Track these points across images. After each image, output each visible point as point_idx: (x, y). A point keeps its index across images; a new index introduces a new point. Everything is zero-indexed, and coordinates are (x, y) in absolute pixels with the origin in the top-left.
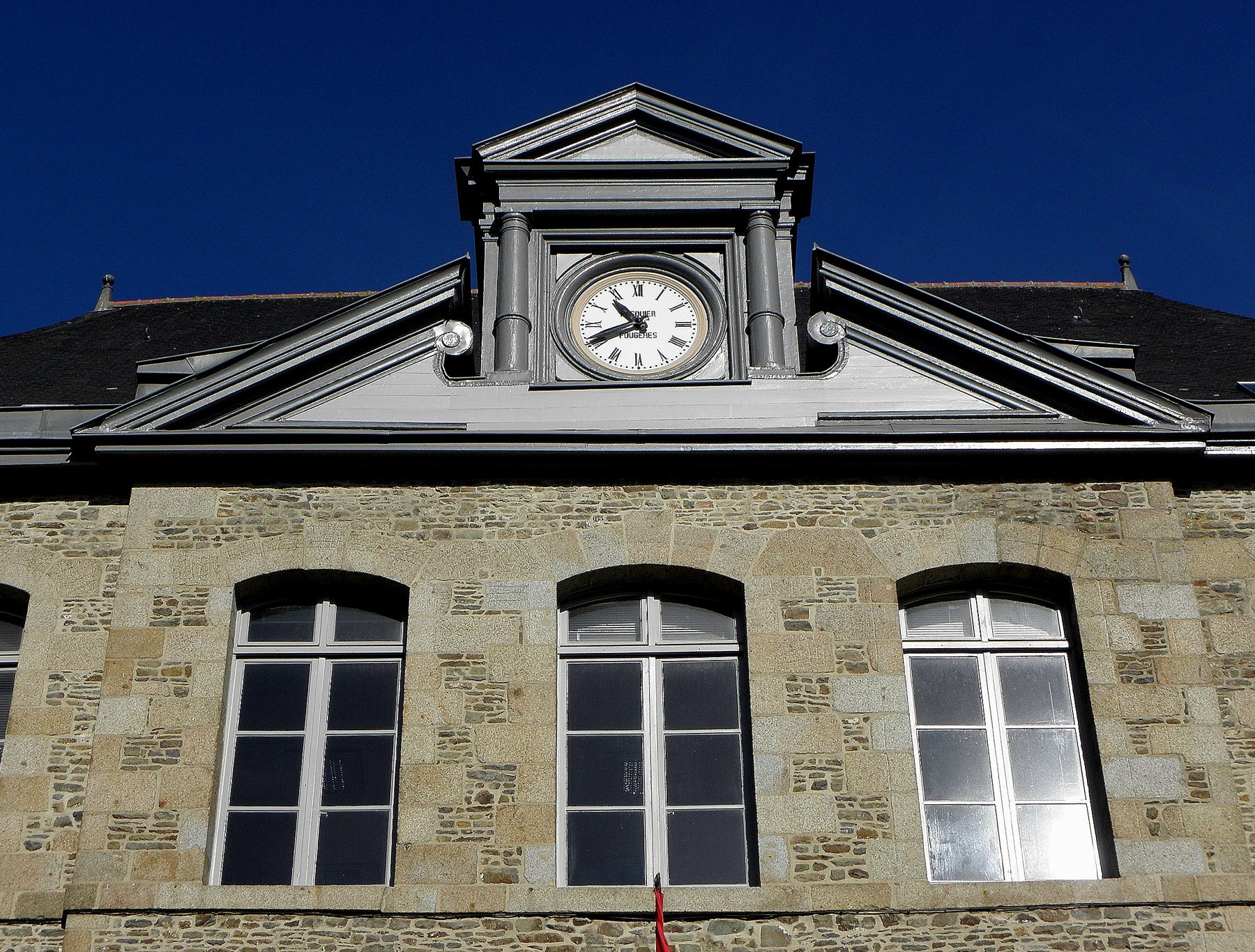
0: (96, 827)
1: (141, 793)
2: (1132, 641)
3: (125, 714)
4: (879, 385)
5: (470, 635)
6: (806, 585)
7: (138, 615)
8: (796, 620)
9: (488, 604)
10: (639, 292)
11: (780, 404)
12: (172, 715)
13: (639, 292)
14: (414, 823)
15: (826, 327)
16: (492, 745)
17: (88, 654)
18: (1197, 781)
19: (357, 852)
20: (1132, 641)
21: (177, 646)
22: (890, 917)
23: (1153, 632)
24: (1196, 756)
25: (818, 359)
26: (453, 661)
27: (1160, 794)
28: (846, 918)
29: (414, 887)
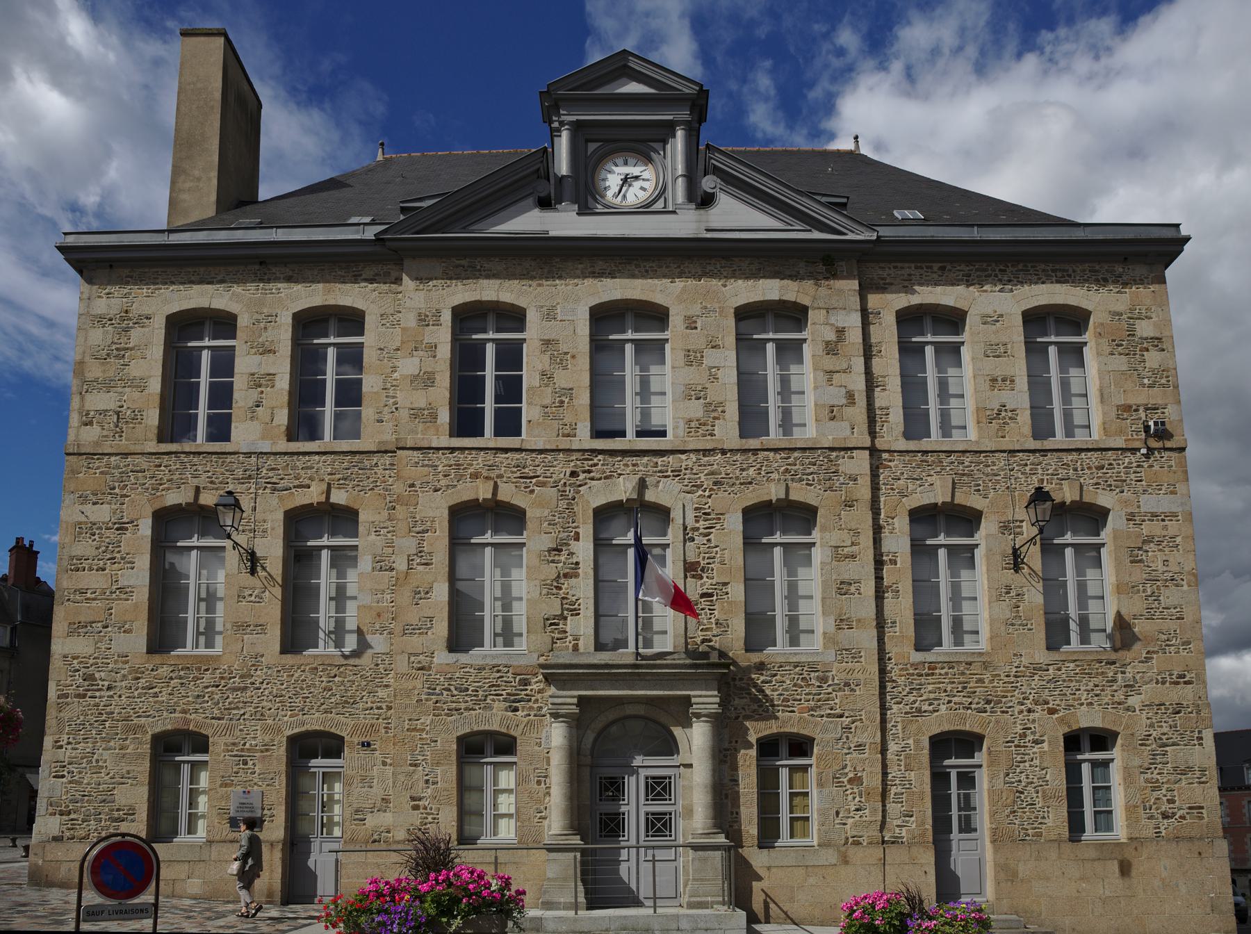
0: (404, 414)
2: (832, 336)
3: (409, 366)
4: (735, 216)
5: (552, 330)
6: (696, 309)
7: (410, 321)
8: (691, 325)
9: (558, 314)
10: (643, 189)
11: (684, 224)
12: (429, 365)
13: (643, 189)
14: (529, 411)
15: (708, 183)
16: (562, 379)
18: (850, 396)
19: (509, 423)
20: (832, 336)
21: (430, 335)
22: (724, 452)
23: (841, 332)
24: (851, 387)
25: (706, 201)
26: (547, 342)
28: (706, 452)
29: (529, 437)
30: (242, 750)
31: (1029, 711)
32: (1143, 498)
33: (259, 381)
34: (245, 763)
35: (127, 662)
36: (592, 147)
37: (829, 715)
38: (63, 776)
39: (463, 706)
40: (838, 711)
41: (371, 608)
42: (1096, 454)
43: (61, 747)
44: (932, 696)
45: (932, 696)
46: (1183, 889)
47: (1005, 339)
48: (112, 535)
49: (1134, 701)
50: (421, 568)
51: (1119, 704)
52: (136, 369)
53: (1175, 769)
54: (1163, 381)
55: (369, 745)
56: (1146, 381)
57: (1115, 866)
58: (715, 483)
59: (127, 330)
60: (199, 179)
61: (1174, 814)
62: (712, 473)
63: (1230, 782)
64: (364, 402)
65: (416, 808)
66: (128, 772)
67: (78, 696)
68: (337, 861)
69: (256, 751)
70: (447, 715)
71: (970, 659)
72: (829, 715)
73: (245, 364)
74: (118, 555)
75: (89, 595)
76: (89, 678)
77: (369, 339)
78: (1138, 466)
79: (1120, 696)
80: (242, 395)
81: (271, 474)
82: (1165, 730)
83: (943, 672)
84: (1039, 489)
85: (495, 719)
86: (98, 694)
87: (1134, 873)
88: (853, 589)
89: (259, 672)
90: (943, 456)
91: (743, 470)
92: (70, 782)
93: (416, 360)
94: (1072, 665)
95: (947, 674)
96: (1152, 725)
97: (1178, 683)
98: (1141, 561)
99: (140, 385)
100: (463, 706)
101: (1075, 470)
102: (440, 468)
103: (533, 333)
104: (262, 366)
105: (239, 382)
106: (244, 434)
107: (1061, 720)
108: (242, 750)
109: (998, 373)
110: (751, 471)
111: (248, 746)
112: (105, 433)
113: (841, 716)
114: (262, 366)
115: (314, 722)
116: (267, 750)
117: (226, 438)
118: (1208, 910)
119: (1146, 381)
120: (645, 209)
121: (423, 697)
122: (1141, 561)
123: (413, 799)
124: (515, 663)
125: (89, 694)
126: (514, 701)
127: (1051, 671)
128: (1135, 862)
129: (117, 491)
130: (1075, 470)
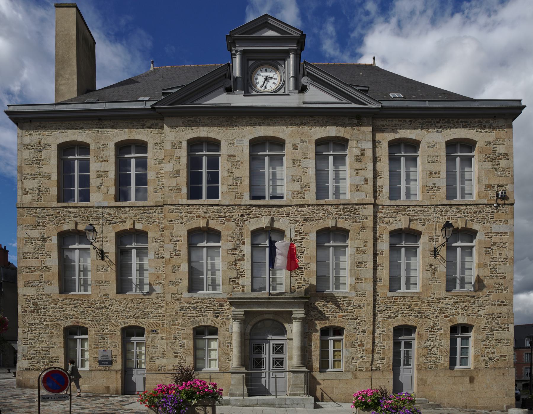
0: (166, 189)
1: (173, 182)
2: (359, 153)
3: (168, 167)
4: (317, 96)
5: (232, 151)
6: (298, 141)
7: (168, 146)
11: (293, 100)
16: (237, 173)
17: (161, 154)
20: (359, 153)
22: (309, 206)
23: (363, 151)
24: (366, 177)
25: (303, 89)
26: (230, 156)
27: (359, 184)
28: (301, 206)
29: (222, 199)
30: (102, 334)
31: (436, 317)
32: (493, 226)
33: (101, 175)
34: (104, 339)
35: (51, 297)
36: (251, 63)
37: (351, 319)
38: (27, 344)
39: (195, 315)
40: (355, 317)
41: (154, 274)
42: (474, 207)
43: (26, 333)
44: (395, 310)
45: (395, 310)
46: (495, 388)
47: (437, 154)
48: (40, 243)
49: (481, 312)
50: (176, 257)
51: (475, 314)
52: (45, 169)
53: (496, 340)
54: (507, 173)
55: (156, 331)
56: (499, 173)
57: (467, 379)
58: (305, 220)
59: (40, 151)
60: (68, 79)
61: (494, 358)
62: (303, 215)
63: (518, 345)
64: (149, 184)
65: (176, 357)
66: (55, 343)
67: (31, 312)
68: (144, 377)
69: (108, 334)
70: (188, 319)
71: (412, 295)
72: (351, 319)
73: (94, 167)
74: (44, 252)
75: (32, 269)
76: (35, 304)
77: (150, 155)
78: (492, 212)
79: (475, 310)
80: (94, 181)
81: (108, 216)
82: (493, 324)
83: (401, 300)
84: (447, 222)
85: (209, 320)
86: (39, 311)
87: (475, 381)
88: (363, 265)
89: (107, 302)
90: (406, 207)
91: (317, 214)
92: (31, 347)
93: (171, 165)
94: (456, 298)
95: (402, 301)
96: (488, 323)
97: (501, 305)
98: (490, 253)
99: (48, 176)
100: (195, 315)
101: (464, 213)
102: (183, 213)
103: (224, 151)
104: (102, 167)
105: (92, 175)
106: (96, 199)
107: (450, 321)
108: (102, 334)
109: (433, 170)
110: (321, 214)
111: (104, 332)
112: (34, 198)
113: (356, 319)
114: (102, 167)
115: (132, 322)
116: (113, 334)
117: (88, 200)
118: (504, 396)
119: (499, 173)
120: (275, 93)
121: (178, 311)
122: (490, 253)
123: (175, 353)
124: (217, 297)
125: (36, 311)
126: (217, 313)
127: (447, 300)
128: (476, 377)
129: (41, 224)
130: (464, 213)
